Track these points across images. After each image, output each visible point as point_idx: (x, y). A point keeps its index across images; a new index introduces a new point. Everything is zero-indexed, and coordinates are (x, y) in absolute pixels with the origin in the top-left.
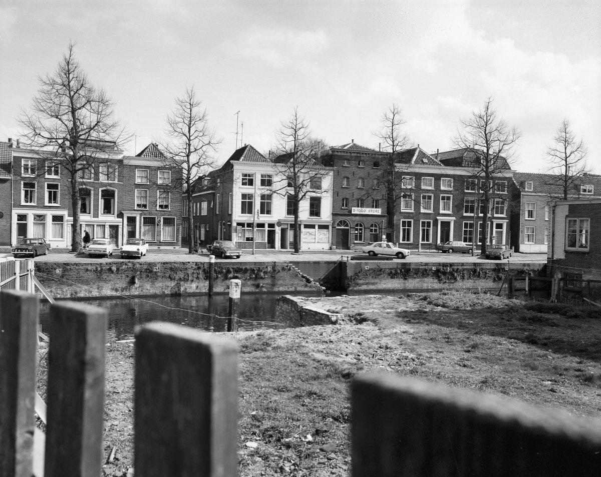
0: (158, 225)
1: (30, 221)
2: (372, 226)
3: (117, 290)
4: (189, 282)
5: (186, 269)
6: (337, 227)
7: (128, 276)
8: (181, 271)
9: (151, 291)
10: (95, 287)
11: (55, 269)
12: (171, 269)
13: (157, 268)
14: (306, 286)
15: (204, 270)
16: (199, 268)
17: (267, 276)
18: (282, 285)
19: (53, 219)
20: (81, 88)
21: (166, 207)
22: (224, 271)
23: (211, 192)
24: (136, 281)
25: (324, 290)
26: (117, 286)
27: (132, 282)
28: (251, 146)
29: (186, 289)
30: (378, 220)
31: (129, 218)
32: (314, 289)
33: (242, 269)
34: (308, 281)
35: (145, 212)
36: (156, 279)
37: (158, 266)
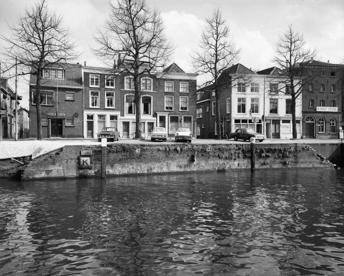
0: (180, 122)
1: (96, 119)
2: (331, 121)
3: (181, 167)
4: (233, 160)
5: (230, 149)
6: (306, 122)
7: (188, 156)
8: (226, 151)
9: (206, 168)
10: (165, 164)
11: (135, 149)
12: (219, 149)
13: (209, 149)
14: (321, 163)
15: (243, 150)
16: (239, 149)
17: (291, 155)
18: (302, 163)
19: (110, 118)
20: (141, 10)
21: (186, 108)
22: (258, 151)
23: (207, 100)
24: (195, 159)
25: (335, 167)
26: (181, 163)
27: (192, 160)
28: (240, 64)
29: (230, 166)
30: (336, 116)
31: (161, 117)
32: (328, 166)
33: (272, 150)
34: (322, 159)
35: (172, 112)
36: (209, 158)
37: (210, 147)
